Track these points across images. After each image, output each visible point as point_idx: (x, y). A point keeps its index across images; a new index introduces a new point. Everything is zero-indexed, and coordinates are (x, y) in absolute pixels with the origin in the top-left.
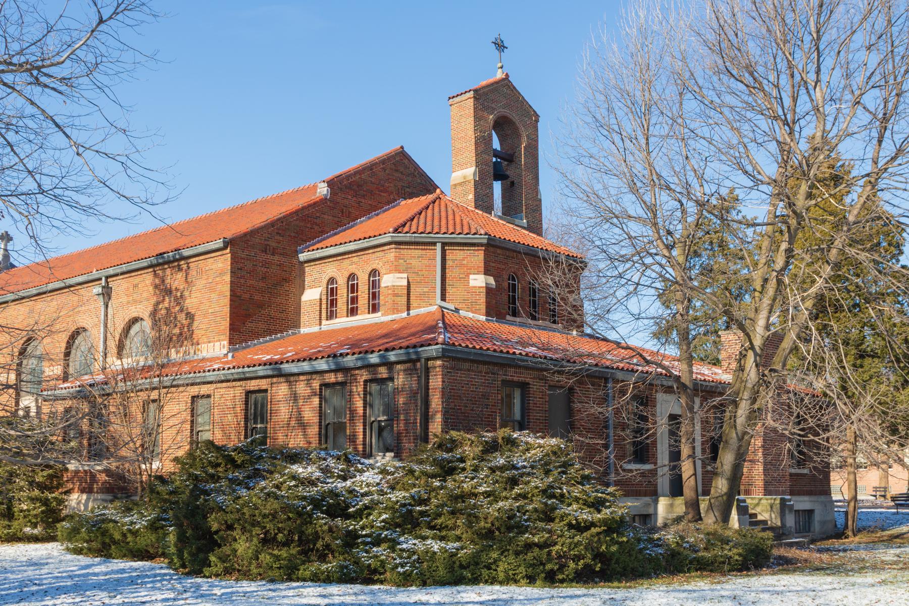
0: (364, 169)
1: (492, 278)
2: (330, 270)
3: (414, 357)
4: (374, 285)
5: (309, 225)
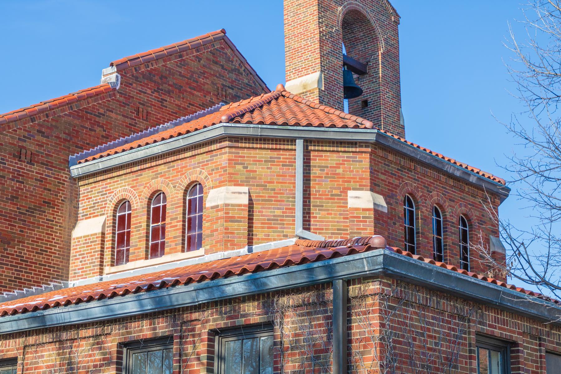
0: (170, 54)
1: (382, 197)
2: (120, 187)
3: (322, 276)
4: (193, 206)
5: (87, 125)
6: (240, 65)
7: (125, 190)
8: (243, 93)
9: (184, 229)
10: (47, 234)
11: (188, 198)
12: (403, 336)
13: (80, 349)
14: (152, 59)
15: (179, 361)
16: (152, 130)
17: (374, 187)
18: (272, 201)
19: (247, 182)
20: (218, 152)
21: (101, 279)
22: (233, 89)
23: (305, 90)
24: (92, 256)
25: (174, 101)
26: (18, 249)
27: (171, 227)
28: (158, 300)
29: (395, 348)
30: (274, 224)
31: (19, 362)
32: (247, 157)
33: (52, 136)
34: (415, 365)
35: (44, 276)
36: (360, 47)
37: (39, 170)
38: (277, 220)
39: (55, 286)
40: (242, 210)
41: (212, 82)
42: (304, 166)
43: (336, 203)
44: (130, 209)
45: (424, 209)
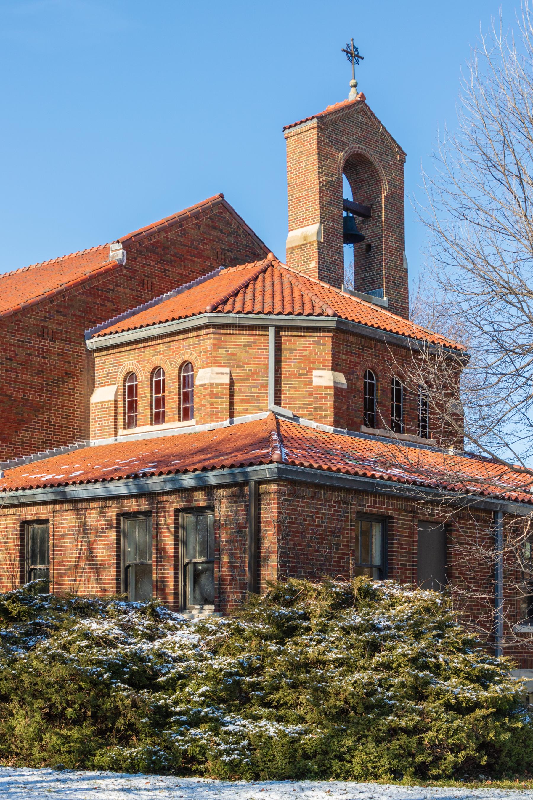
0: (171, 225)
1: (342, 374)
2: (128, 361)
3: (240, 479)
5: (99, 301)
6: (238, 227)
7: (132, 364)
8: (241, 255)
9: (179, 401)
10: (70, 401)
11: (182, 374)
12: (296, 519)
13: (92, 516)
14: (155, 232)
15: (156, 529)
16: (157, 300)
17: (335, 367)
18: (249, 380)
19: (229, 363)
20: (205, 337)
21: (116, 440)
22: (232, 252)
23: (305, 242)
24: (107, 420)
25: (176, 270)
26: (47, 415)
27: (170, 399)
28: (140, 487)
29: (289, 527)
30: (252, 399)
31: (51, 522)
32: (229, 342)
33: (69, 314)
34: (305, 537)
35: (69, 437)
36: (365, 189)
37: (60, 346)
38: (254, 396)
39: (79, 445)
40: (225, 388)
41: (212, 248)
42: (275, 349)
43: (303, 381)
44: (136, 381)
45: (383, 381)
